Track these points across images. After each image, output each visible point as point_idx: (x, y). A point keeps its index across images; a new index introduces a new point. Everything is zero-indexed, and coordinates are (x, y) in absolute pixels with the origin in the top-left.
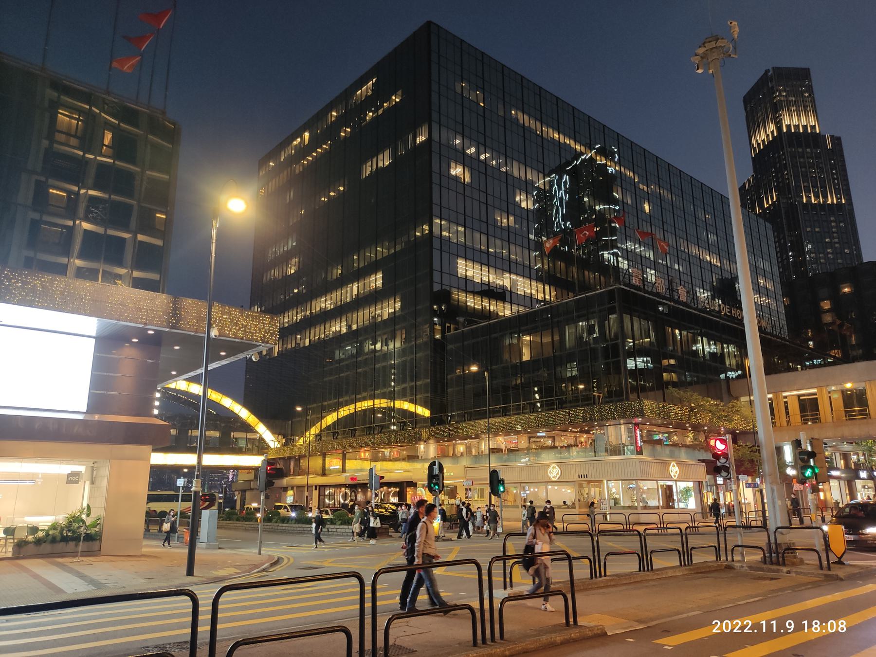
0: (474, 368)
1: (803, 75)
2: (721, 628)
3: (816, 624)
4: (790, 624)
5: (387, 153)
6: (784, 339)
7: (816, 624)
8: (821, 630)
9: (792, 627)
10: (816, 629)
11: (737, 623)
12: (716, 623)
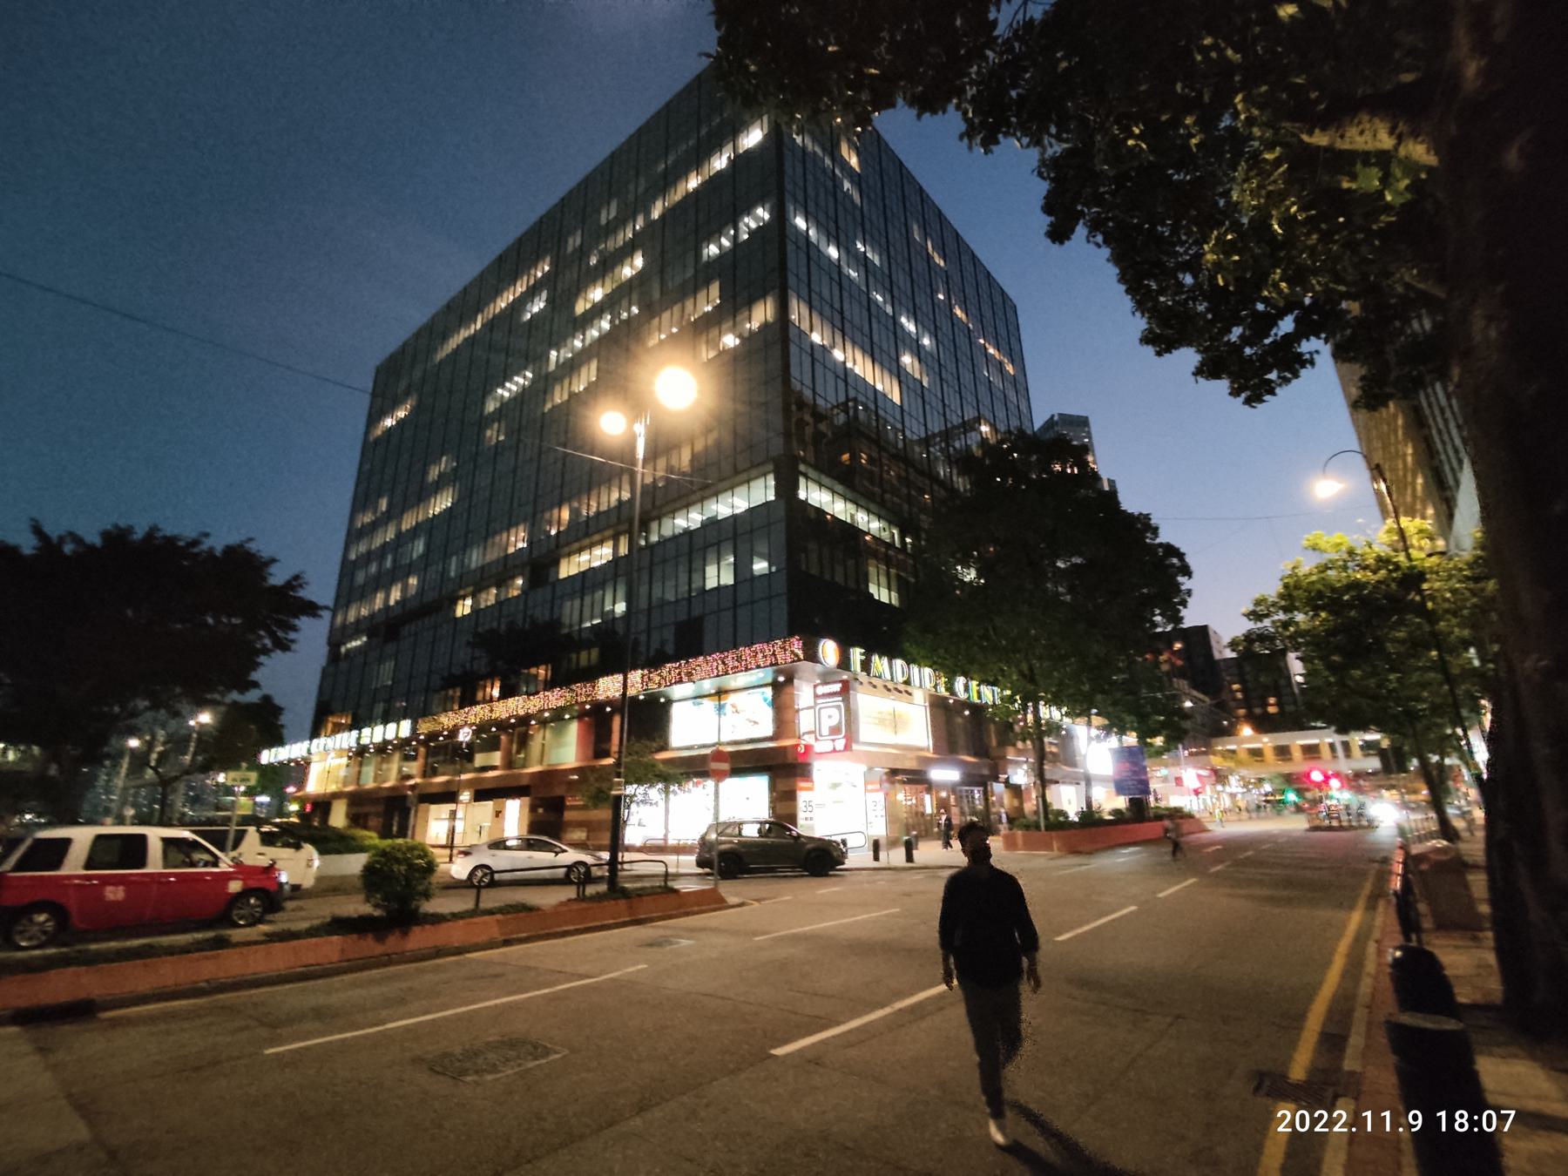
0: (1512, 158)
1: (297, 577)
2: (1292, 1124)
3: (1462, 1125)
4: (1415, 1117)
5: (548, 259)
6: (807, 478)
7: (1462, 1116)
8: (1471, 1128)
9: (1420, 1122)
10: (1462, 1125)
11: (1321, 1116)
12: (1284, 1116)
